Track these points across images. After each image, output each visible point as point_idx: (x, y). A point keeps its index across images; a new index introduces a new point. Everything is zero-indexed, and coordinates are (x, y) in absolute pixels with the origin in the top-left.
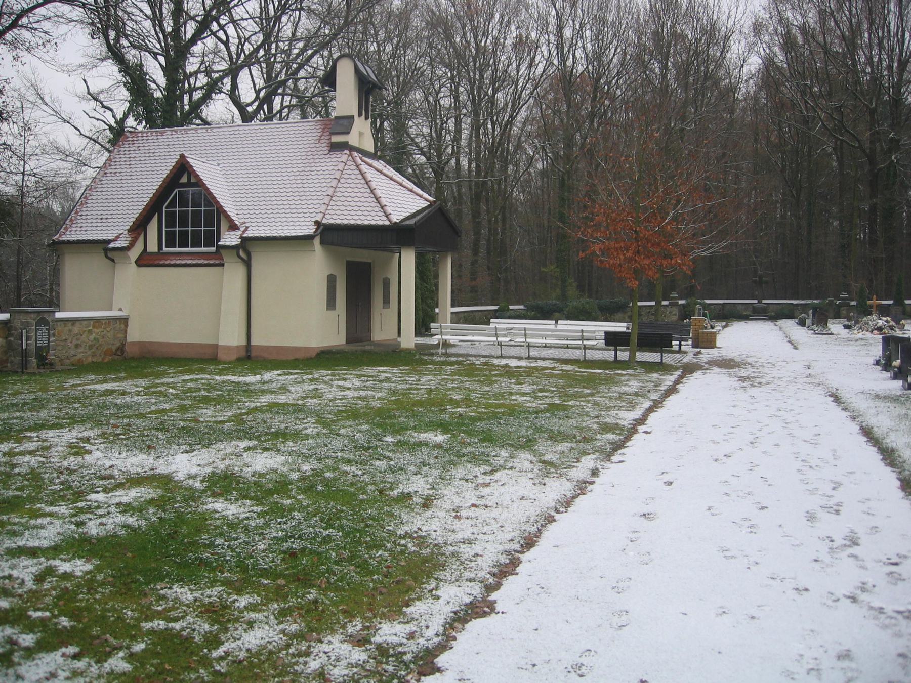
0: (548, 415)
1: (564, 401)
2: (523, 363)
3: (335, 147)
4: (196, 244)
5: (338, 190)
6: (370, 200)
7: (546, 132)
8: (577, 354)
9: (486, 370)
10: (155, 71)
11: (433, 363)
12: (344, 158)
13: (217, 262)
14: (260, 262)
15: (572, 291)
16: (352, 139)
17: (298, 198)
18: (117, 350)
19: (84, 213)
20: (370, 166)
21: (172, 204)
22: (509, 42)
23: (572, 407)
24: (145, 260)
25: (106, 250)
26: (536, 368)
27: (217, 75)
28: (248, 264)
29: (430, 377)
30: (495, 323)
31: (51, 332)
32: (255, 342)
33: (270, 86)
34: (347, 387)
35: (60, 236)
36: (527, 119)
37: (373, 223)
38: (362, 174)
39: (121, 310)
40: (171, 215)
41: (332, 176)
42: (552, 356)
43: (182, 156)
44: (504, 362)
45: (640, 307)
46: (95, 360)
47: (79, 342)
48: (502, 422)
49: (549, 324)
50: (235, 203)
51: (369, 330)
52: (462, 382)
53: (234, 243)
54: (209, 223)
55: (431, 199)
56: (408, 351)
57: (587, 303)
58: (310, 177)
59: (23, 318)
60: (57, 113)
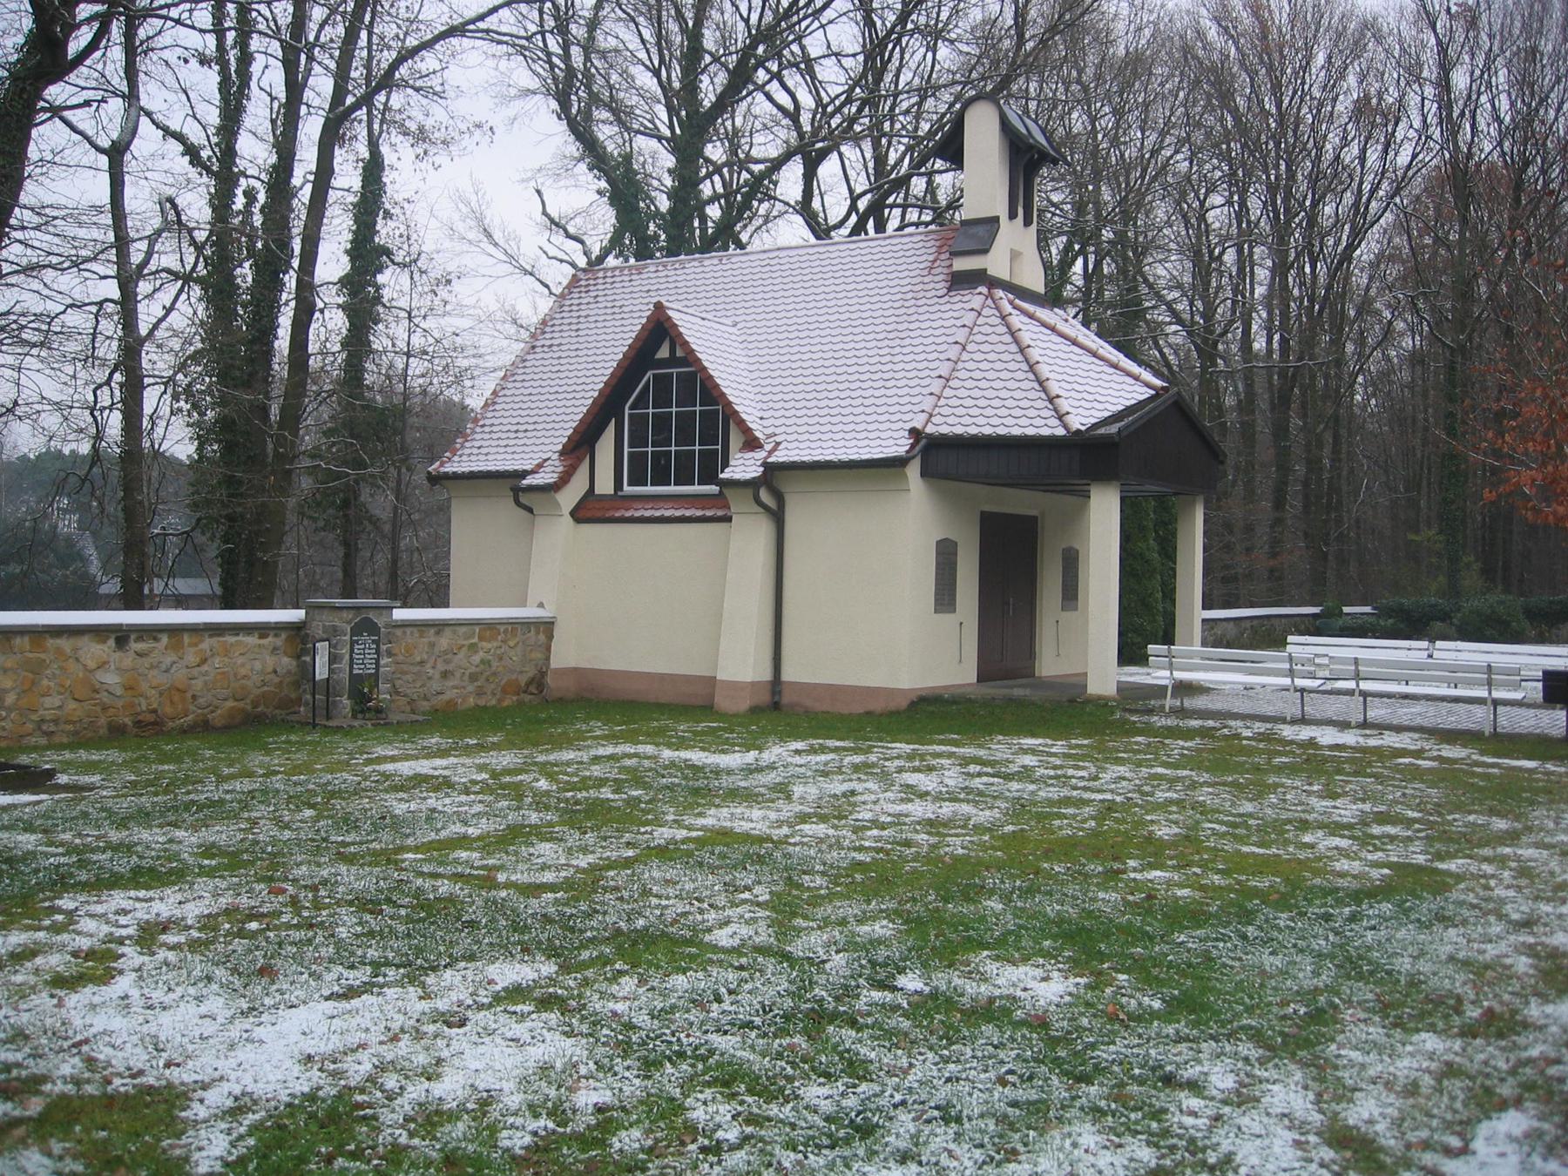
0: (1386, 907)
1: (1440, 857)
2: (1350, 738)
3: (961, 281)
5: (960, 365)
6: (1026, 385)
7: (1418, 273)
8: (1478, 718)
9: (1263, 752)
10: (656, 160)
11: (1148, 730)
12: (977, 301)
13: (720, 513)
15: (1471, 579)
16: (996, 263)
17: (881, 383)
18: (528, 684)
19: (488, 422)
20: (1031, 316)
21: (641, 402)
22: (1344, 106)
23: (1459, 878)
24: (590, 511)
26: (1376, 750)
27: (761, 167)
28: (778, 517)
29: (1122, 770)
30: (1300, 646)
31: (384, 648)
32: (788, 675)
33: (882, 186)
34: (927, 795)
35: (442, 465)
36: (1380, 257)
37: (1030, 432)
38: (1013, 333)
39: (541, 605)
40: (638, 422)
41: (951, 339)
42: (1418, 721)
43: (659, 307)
44: (1305, 733)
46: (482, 702)
47: (450, 667)
48: (1251, 931)
49: (1409, 651)
50: (759, 397)
51: (1031, 654)
52: (1194, 785)
53: (748, 476)
54: (709, 437)
55: (1158, 383)
56: (1101, 703)
57: (1502, 602)
58: (908, 341)
59: (329, 619)
60: (511, 258)
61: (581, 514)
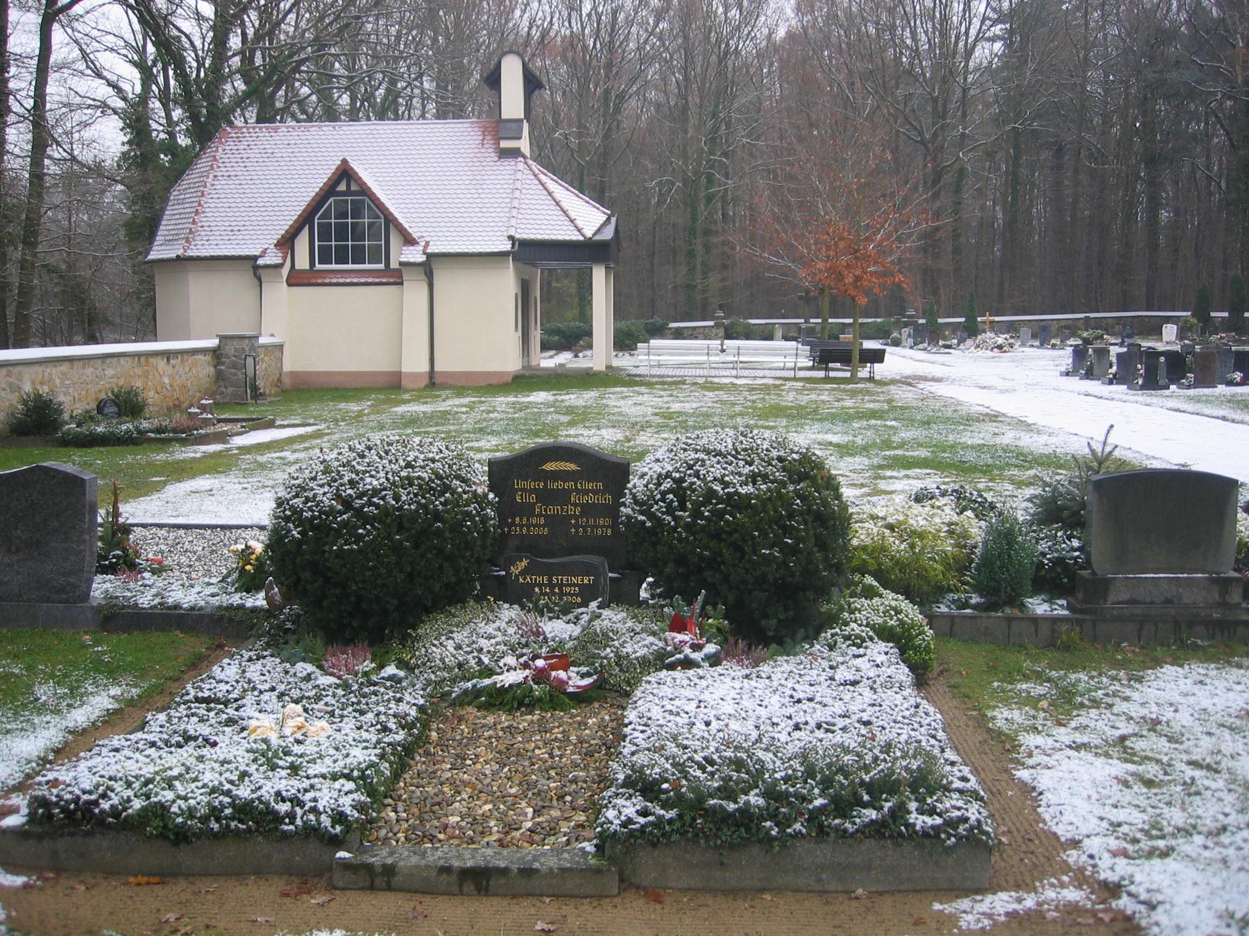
3: (505, 154)
4: (342, 260)
14: (442, 279)
21: (326, 215)
24: (297, 279)
25: (256, 268)
32: (436, 369)
39: (272, 335)
43: (344, 161)
45: (862, 324)
61: (292, 281)
